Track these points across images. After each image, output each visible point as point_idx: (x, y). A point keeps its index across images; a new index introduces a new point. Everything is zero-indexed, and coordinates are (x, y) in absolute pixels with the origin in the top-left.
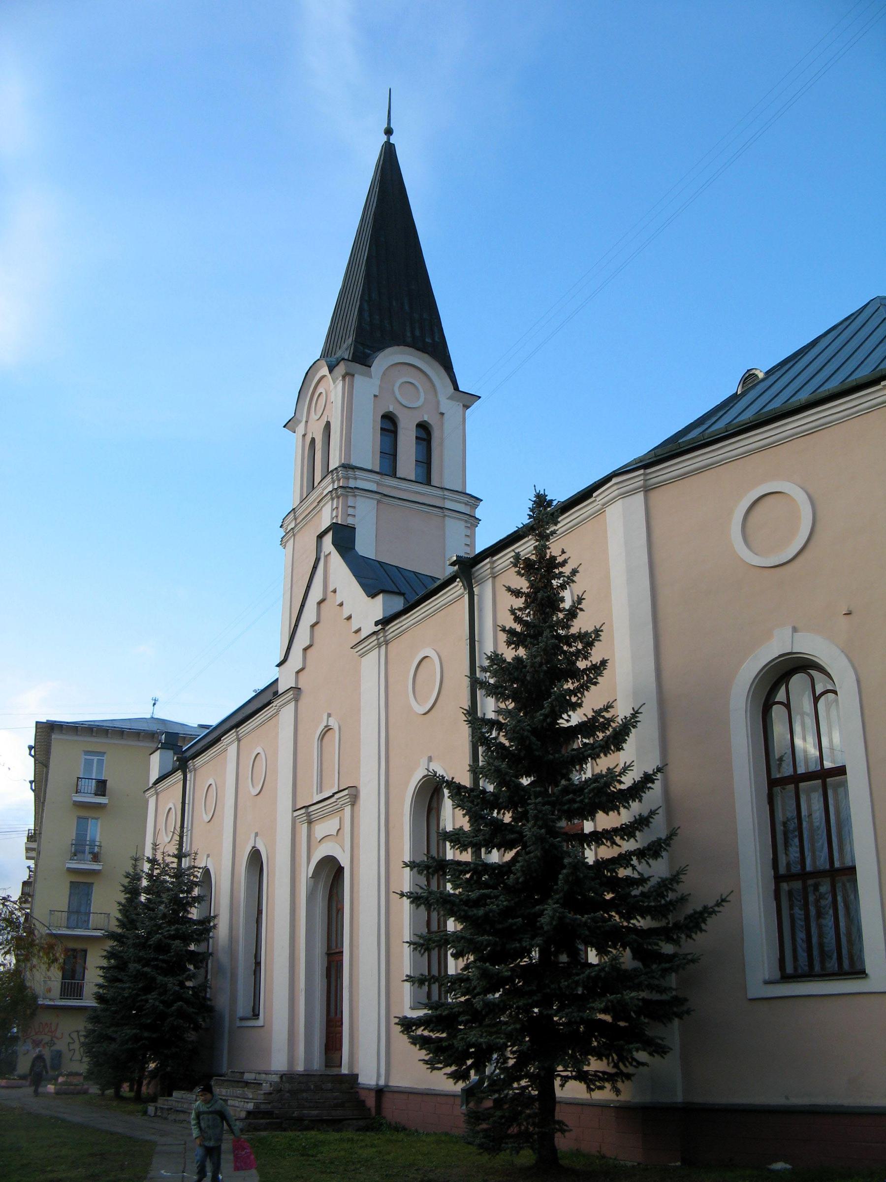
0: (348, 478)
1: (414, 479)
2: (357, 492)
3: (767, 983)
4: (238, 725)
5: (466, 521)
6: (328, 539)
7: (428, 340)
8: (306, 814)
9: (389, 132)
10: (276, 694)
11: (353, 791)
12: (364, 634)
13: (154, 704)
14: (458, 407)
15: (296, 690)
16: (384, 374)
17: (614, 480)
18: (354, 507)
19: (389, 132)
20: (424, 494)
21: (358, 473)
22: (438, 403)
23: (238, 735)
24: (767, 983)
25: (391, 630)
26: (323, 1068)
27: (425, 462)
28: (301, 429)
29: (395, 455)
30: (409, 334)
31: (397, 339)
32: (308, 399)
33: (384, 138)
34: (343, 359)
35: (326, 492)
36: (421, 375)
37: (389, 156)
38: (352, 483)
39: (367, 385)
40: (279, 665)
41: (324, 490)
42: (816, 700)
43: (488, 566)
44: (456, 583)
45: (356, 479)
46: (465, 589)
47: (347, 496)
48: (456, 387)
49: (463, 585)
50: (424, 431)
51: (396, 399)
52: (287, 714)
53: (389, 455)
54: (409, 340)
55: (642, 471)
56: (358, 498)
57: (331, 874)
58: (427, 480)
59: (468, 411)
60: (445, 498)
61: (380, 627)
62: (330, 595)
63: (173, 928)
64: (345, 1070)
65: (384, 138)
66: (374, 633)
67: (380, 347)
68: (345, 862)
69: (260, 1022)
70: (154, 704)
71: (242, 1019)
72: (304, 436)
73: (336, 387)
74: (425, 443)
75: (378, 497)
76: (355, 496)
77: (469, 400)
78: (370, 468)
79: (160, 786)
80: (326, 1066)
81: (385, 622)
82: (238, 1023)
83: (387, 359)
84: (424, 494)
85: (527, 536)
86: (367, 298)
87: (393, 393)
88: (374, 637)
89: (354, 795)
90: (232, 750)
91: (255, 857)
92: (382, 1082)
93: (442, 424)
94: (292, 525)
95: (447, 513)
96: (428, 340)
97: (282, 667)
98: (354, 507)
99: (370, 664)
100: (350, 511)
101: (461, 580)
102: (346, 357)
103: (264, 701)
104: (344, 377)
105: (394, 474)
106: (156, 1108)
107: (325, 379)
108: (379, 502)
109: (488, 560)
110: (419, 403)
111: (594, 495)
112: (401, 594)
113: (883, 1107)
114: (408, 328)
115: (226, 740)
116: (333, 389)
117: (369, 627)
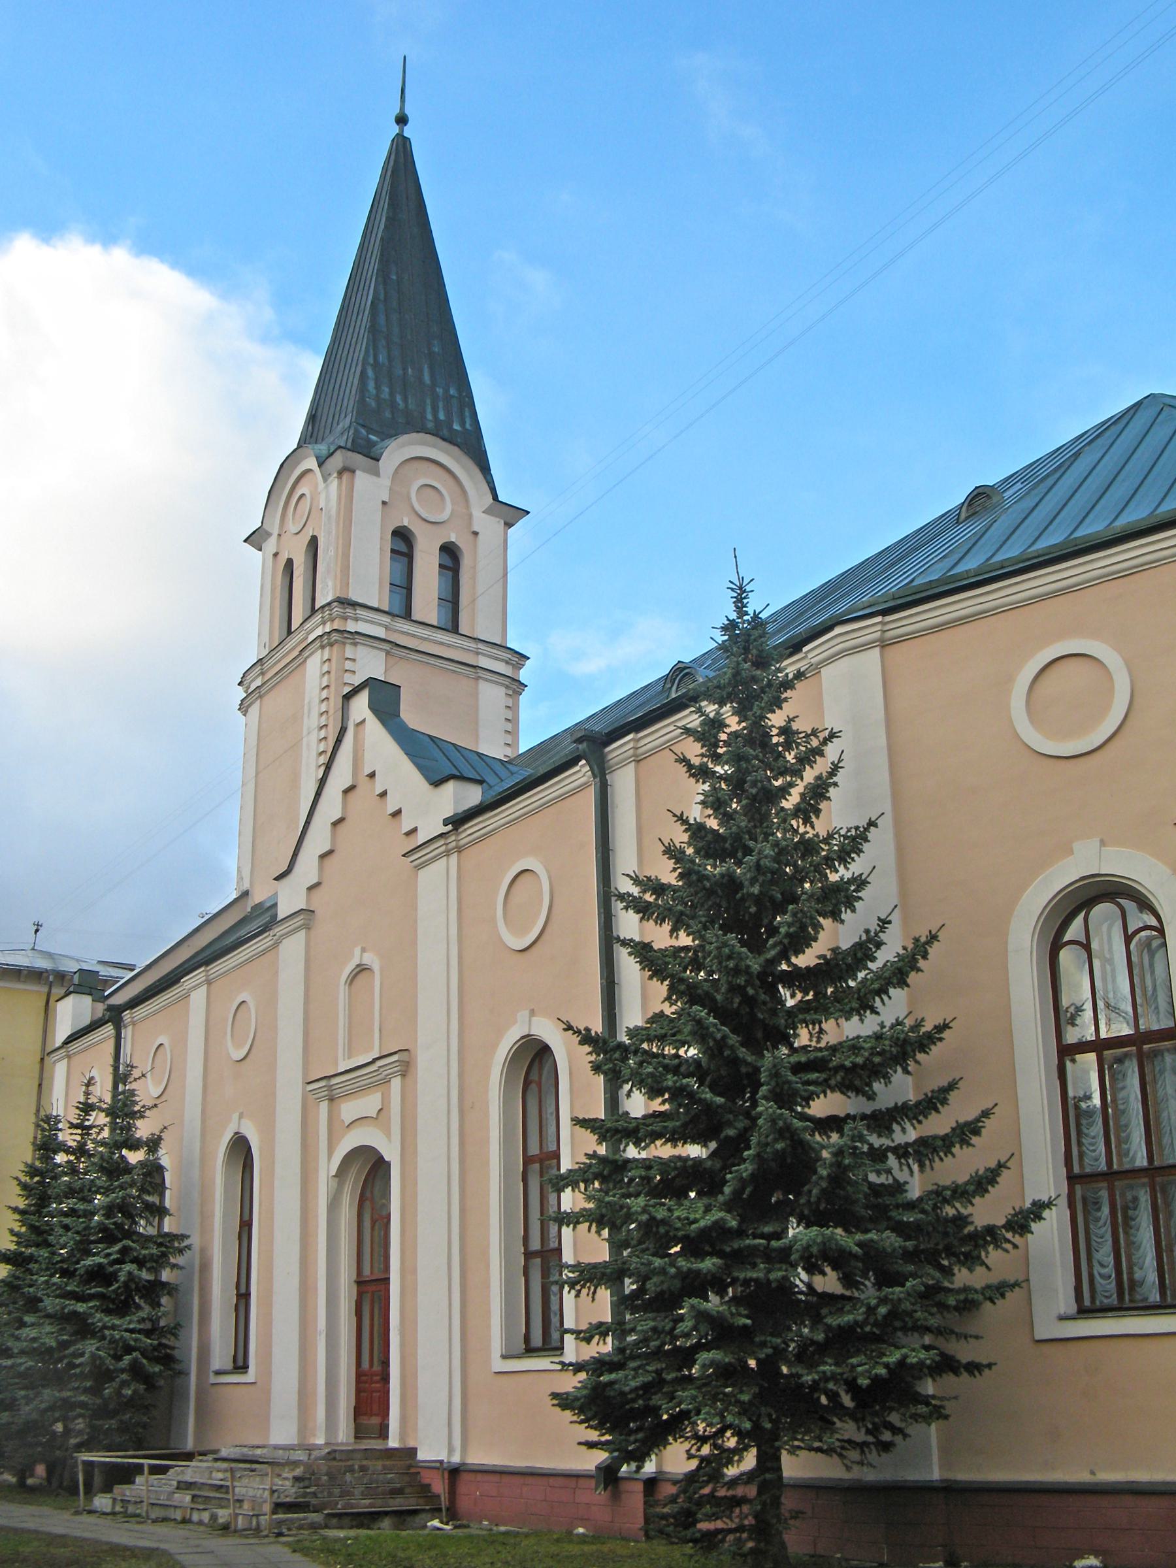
0: (346, 619)
1: (435, 624)
2: (359, 639)
3: (1063, 1318)
4: (207, 962)
5: (507, 687)
6: (363, 699)
7: (456, 427)
8: (327, 1088)
9: (402, 120)
10: (273, 922)
11: (404, 1056)
12: (421, 838)
13: (37, 931)
14: (496, 524)
15: (308, 912)
16: (396, 471)
17: (838, 630)
18: (354, 660)
19: (402, 120)
20: (448, 646)
21: (360, 612)
22: (470, 516)
23: (207, 976)
24: (1063, 1318)
25: (469, 832)
26: (353, 1440)
27: (452, 601)
28: (271, 545)
29: (409, 589)
30: (430, 417)
31: (413, 424)
32: (282, 503)
33: (396, 129)
34: (340, 447)
35: (311, 637)
36: (446, 476)
37: (401, 162)
38: (351, 626)
39: (370, 487)
40: (277, 879)
41: (309, 634)
42: (1128, 939)
43: (631, 745)
44: (577, 768)
45: (356, 620)
46: (594, 776)
47: (344, 644)
48: (495, 497)
49: (592, 769)
50: (450, 552)
51: (413, 508)
52: (292, 949)
53: (404, 588)
54: (430, 425)
55: (879, 619)
56: (360, 647)
57: (369, 1171)
58: (453, 627)
59: (511, 531)
60: (478, 653)
61: (450, 827)
62: (363, 782)
63: (117, 1248)
64: (393, 1442)
65: (396, 129)
66: (441, 835)
67: (391, 431)
68: (391, 1153)
69: (251, 1376)
70: (37, 931)
71: (218, 1373)
72: (276, 555)
73: (327, 487)
74: (450, 573)
75: (387, 647)
76: (355, 644)
77: (512, 515)
78: (376, 605)
79: (74, 1047)
80: (356, 1438)
81: (458, 821)
82: (213, 1379)
83: (399, 451)
84: (448, 646)
85: (686, 707)
86: (371, 361)
87: (409, 499)
88: (442, 842)
89: (403, 1063)
90: (198, 997)
91: (240, 1148)
92: (456, 1459)
93: (475, 546)
94: (258, 682)
95: (481, 673)
96: (456, 427)
97: (285, 881)
98: (354, 660)
99: (436, 881)
100: (348, 665)
101: (588, 762)
102: (342, 444)
103: (242, 929)
104: (340, 473)
105: (407, 614)
106: (114, 1500)
107: (309, 476)
108: (388, 653)
109: (631, 736)
110: (444, 516)
111: (805, 649)
112: (480, 782)
113: (1174, 1483)
114: (429, 409)
115: (188, 981)
116: (323, 491)
117: (431, 826)
